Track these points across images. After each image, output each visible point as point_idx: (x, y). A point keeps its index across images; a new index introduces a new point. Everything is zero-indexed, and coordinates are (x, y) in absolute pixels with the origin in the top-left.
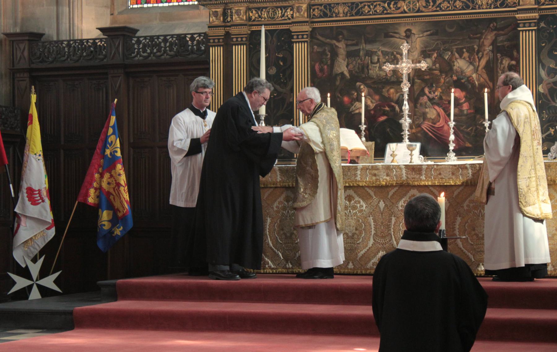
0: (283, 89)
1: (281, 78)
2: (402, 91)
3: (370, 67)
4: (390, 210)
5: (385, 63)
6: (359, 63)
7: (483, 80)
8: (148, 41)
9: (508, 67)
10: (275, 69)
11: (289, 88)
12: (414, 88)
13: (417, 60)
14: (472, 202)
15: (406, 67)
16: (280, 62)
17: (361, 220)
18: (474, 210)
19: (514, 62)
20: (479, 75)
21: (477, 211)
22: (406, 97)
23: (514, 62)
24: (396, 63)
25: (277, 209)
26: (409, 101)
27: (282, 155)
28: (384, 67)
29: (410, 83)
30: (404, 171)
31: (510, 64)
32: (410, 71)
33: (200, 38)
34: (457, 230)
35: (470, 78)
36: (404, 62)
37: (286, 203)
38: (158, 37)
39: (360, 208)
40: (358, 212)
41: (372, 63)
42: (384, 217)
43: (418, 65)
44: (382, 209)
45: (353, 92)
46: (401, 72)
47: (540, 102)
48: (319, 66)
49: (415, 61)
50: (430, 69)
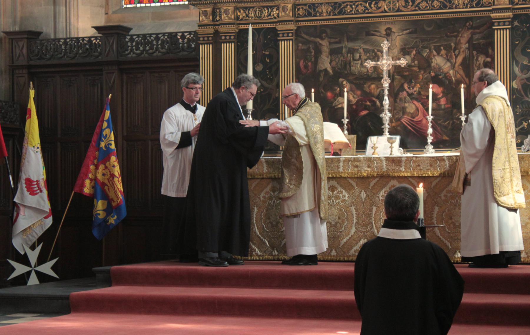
0: (269, 84)
1: (267, 75)
2: (383, 87)
3: (352, 64)
4: (371, 200)
5: (366, 60)
6: (341, 60)
7: (460, 76)
8: (140, 39)
9: (483, 63)
10: (262, 65)
11: (275, 84)
12: (394, 84)
13: (396, 57)
14: (449, 192)
15: (386, 64)
16: (267, 59)
17: (343, 210)
18: (451, 200)
19: (489, 59)
20: (456, 71)
21: (454, 201)
22: (386, 92)
23: (489, 59)
24: (376, 60)
25: (263, 199)
26: (389, 96)
27: (269, 147)
28: (366, 64)
29: (390, 79)
30: (384, 163)
31: (486, 61)
32: (390, 68)
33: (190, 36)
34: (435, 219)
35: (448, 74)
36: (385, 59)
37: (272, 193)
38: (150, 35)
39: (343, 197)
40: (340, 202)
41: (354, 60)
42: (365, 206)
43: (398, 62)
44: (363, 199)
45: (336, 88)
46: (381, 68)
47: (514, 97)
48: (303, 62)
49: (395, 58)
50: (409, 66)
